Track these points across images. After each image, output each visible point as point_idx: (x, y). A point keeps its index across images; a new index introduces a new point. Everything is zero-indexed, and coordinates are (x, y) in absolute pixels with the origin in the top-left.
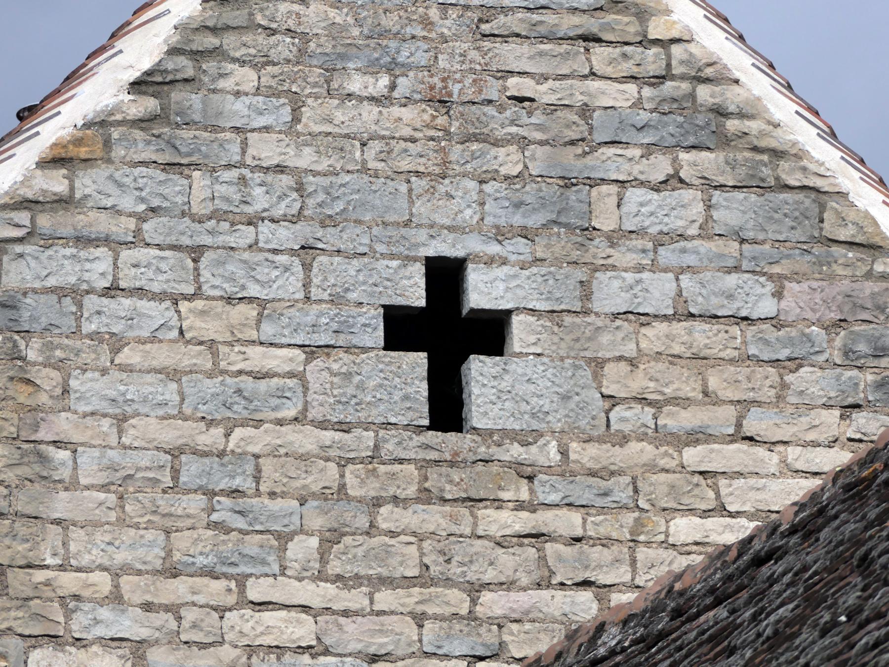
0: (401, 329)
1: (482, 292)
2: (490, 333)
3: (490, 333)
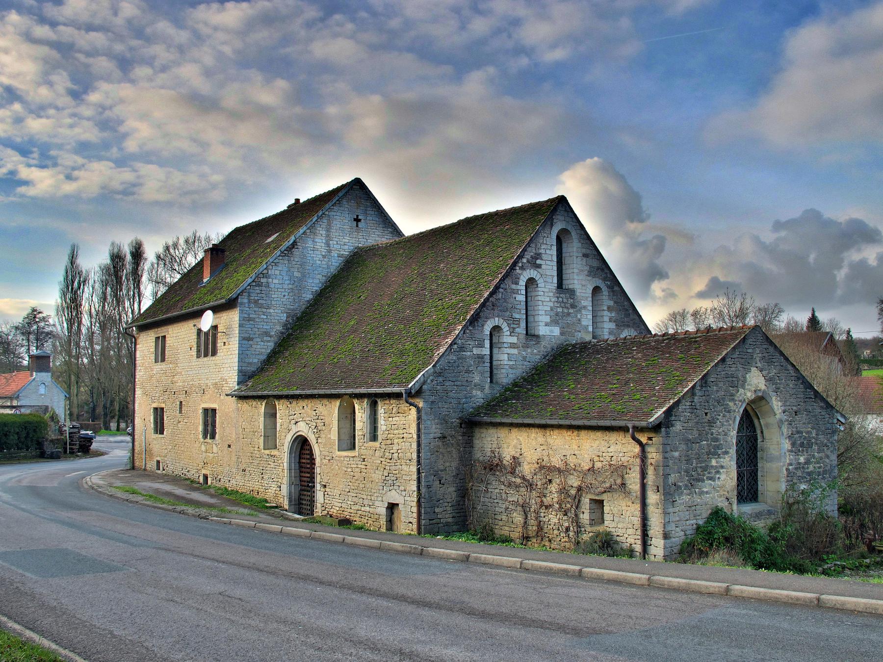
0: (355, 220)
1: (360, 217)
2: (360, 220)
3: (360, 220)
